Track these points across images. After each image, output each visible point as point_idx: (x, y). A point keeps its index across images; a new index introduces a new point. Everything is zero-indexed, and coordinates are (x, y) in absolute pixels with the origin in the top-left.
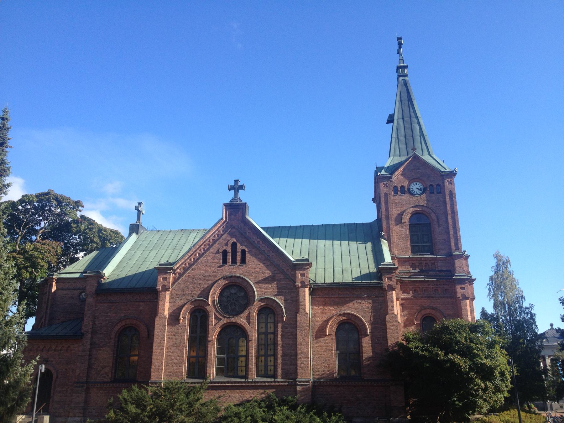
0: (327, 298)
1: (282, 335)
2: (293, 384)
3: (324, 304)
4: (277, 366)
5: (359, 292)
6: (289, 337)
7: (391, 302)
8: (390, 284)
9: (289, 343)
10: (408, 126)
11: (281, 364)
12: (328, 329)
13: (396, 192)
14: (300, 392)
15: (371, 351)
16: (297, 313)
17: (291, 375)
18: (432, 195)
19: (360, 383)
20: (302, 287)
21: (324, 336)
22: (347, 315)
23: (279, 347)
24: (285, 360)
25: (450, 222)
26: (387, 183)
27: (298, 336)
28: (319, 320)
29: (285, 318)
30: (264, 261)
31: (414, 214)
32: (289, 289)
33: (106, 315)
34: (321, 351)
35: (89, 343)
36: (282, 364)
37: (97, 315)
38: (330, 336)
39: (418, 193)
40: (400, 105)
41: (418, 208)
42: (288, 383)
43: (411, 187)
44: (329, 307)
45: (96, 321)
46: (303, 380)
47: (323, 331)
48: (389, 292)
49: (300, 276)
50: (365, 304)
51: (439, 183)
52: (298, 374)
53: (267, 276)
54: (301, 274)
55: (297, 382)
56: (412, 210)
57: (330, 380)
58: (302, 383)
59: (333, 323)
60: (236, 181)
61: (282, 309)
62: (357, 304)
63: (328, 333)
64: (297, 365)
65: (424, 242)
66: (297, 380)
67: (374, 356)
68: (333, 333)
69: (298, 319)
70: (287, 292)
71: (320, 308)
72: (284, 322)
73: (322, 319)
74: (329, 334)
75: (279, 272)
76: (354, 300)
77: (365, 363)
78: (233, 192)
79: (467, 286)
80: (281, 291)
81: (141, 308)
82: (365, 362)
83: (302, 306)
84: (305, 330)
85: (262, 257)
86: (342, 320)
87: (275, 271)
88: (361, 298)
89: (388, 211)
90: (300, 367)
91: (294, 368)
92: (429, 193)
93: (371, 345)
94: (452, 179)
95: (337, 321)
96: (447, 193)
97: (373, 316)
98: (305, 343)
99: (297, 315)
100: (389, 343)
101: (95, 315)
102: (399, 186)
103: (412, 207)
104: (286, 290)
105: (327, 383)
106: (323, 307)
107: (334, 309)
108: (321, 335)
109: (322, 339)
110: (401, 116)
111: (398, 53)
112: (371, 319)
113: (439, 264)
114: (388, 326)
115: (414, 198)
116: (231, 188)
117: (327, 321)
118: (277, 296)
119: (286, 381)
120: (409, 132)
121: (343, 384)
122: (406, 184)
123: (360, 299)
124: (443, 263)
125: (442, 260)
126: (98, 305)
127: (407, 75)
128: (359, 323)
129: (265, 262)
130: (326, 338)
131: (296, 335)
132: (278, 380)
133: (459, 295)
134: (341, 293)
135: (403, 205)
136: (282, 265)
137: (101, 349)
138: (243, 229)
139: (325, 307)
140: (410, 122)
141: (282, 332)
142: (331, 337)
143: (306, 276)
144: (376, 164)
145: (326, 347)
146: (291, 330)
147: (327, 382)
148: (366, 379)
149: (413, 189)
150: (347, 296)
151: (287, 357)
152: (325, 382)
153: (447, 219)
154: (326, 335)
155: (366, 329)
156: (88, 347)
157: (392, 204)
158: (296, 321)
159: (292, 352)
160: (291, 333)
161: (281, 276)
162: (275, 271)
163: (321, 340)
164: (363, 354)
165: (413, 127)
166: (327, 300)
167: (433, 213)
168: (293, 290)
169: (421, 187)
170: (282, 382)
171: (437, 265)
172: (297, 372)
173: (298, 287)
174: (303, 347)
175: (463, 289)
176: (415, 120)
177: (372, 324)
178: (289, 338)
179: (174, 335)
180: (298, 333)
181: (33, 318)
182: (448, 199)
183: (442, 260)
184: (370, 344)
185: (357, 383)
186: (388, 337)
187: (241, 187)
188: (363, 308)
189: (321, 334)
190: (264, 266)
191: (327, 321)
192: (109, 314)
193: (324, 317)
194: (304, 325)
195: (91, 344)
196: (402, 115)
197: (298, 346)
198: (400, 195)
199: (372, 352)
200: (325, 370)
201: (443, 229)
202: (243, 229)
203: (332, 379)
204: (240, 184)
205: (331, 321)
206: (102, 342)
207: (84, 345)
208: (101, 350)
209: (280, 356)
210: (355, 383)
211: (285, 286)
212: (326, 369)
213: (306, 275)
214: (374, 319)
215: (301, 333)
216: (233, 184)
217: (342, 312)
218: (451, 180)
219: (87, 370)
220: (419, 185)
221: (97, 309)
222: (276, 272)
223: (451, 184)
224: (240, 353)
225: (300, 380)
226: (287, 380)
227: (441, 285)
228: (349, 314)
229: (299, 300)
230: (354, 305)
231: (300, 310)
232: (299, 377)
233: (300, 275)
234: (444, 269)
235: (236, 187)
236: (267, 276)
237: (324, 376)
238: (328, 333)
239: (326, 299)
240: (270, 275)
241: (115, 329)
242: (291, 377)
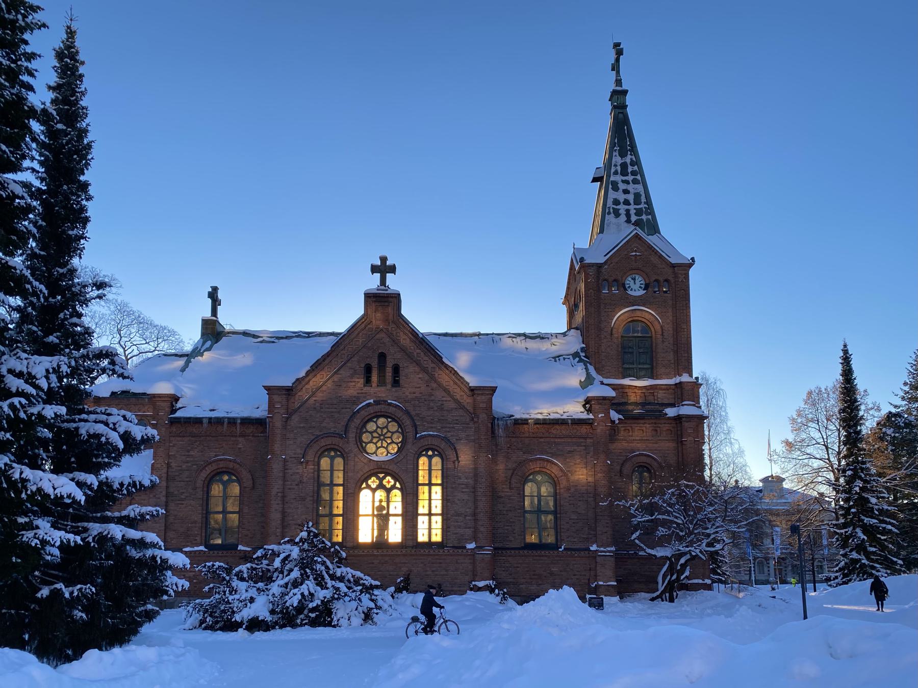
6: (464, 490)
32: (462, 424)
33: (187, 453)
35: (164, 493)
37: (173, 453)
43: (628, 282)
45: (171, 463)
60: (384, 259)
65: (640, 364)
78: (377, 276)
81: (240, 446)
101: (170, 454)
108: (503, 488)
111: (613, 69)
113: (659, 396)
116: (374, 269)
124: (665, 393)
125: (664, 389)
126: (172, 439)
137: (183, 502)
138: (395, 334)
144: (846, 360)
146: (466, 480)
151: (461, 518)
156: (164, 499)
159: (468, 510)
168: (469, 426)
169: (630, 279)
178: (463, 492)
179: (297, 485)
181: (131, 456)
187: (393, 269)
189: (504, 486)
192: (192, 453)
195: (167, 496)
202: (395, 334)
204: (379, 263)
206: (184, 493)
207: (157, 496)
208: (183, 504)
211: (457, 420)
216: (378, 262)
219: (527, 526)
221: (171, 444)
222: (444, 399)
224: (336, 512)
235: (384, 269)
241: (202, 474)
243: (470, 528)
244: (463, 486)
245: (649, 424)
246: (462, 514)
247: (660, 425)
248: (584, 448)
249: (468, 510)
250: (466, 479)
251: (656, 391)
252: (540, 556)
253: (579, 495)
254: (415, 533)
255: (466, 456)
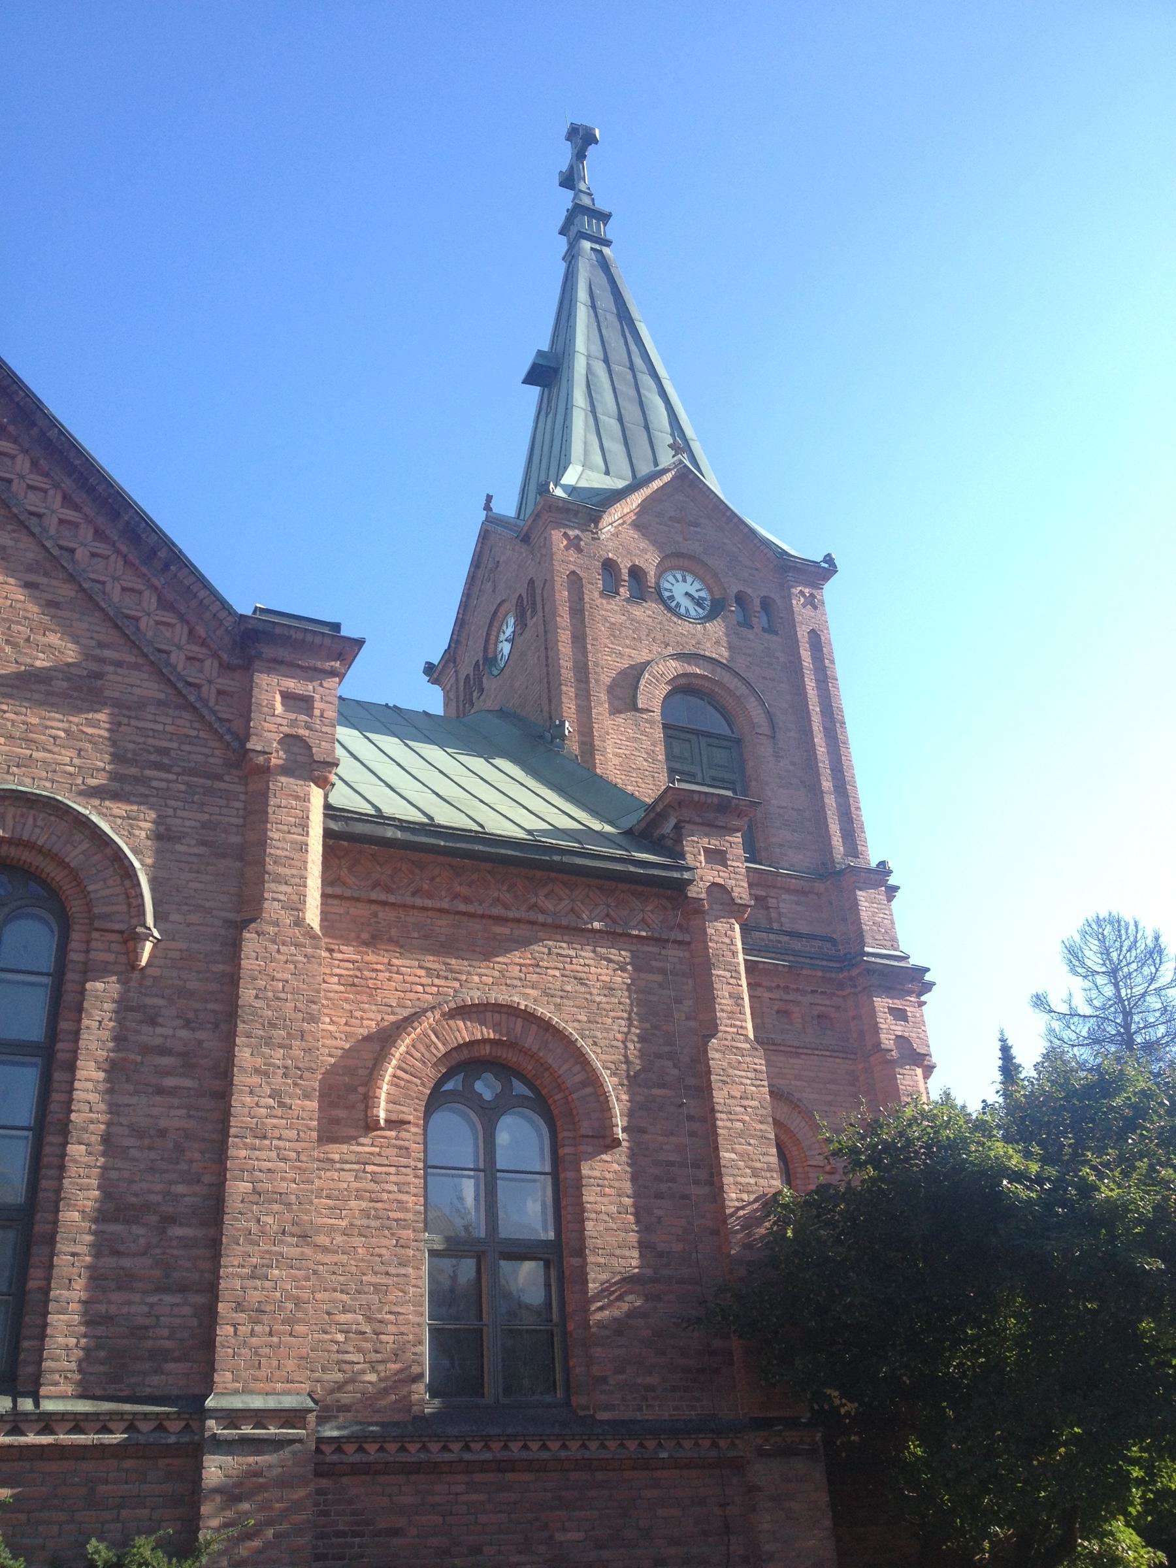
0: (384, 903)
1: (115, 1070)
2: (172, 1439)
3: (365, 936)
4: (47, 1290)
5: (561, 899)
6: (170, 1082)
7: (728, 974)
8: (721, 881)
9: (163, 1123)
10: (627, 390)
11: (79, 1284)
12: (385, 1087)
13: (610, 590)
14: (231, 1494)
15: (633, 1238)
16: (244, 924)
17: (158, 1371)
18: (745, 632)
19: (574, 1445)
20: (286, 771)
21: (352, 1132)
22: (497, 1016)
23: (76, 1150)
24: (117, 1253)
25: (819, 740)
26: (577, 537)
27: (241, 1079)
28: (331, 1028)
29: (148, 946)
30: (30, 569)
31: (683, 688)
32: (192, 772)
34: (332, 1229)
36: (97, 1278)
38: (393, 1134)
39: (693, 613)
40: (593, 320)
41: (697, 666)
42: (131, 1428)
44: (395, 961)
46: (257, 1403)
47: (352, 1097)
48: (716, 920)
49: (279, 708)
50: (593, 969)
51: (773, 596)
52: (223, 1354)
53: (42, 662)
54: (287, 696)
55: (211, 1423)
56: (675, 669)
57: (382, 1425)
58: (247, 1430)
59: (418, 1055)
61: (139, 885)
62: (551, 965)
63: (382, 1115)
64: (212, 1290)
66: (210, 1403)
67: (649, 1272)
68: (413, 1113)
69: (249, 964)
70: (182, 787)
71: (340, 956)
72: (136, 975)
73: (346, 1024)
74: (386, 1121)
75: (133, 659)
76: (537, 940)
77: (598, 1316)
79: (907, 1004)
80: (133, 771)
82: (601, 1309)
83: (284, 888)
84: (296, 1043)
85: (21, 545)
86: (472, 1043)
87: (101, 645)
88: (575, 932)
89: (585, 648)
90: (239, 1307)
91: (187, 1310)
92: (735, 623)
93: (634, 1205)
94: (815, 592)
95: (440, 1045)
96: (802, 633)
97: (638, 1036)
98: (287, 1133)
99: (246, 935)
100: (732, 1197)
102: (624, 565)
103: (678, 657)
104: (172, 777)
105: (360, 1449)
106: (359, 953)
107: (422, 972)
109: (344, 1148)
110: (597, 350)
112: (626, 1056)
113: (784, 908)
114: (719, 1096)
115: (684, 627)
117: (385, 1039)
118: (102, 799)
119: (111, 1414)
120: (632, 413)
121: (467, 1456)
122: (650, 561)
123: (566, 938)
124: (798, 903)
125: (795, 892)
127: (607, 243)
128: (564, 1068)
129: (33, 578)
130: (365, 1146)
131: (224, 1070)
132: (48, 1406)
133: (887, 1041)
134: (463, 890)
135: (640, 640)
136: (158, 623)
139: (371, 958)
140: (633, 380)
141: (115, 1039)
142: (397, 1138)
143: (317, 712)
145: (364, 1205)
146: (184, 1034)
147: (360, 1441)
148: (603, 1416)
149: (675, 594)
150: (497, 911)
151: (137, 1230)
152: (348, 1439)
153: (807, 733)
154: (370, 1126)
155: (606, 1108)
157: (598, 631)
158: (232, 980)
159: (180, 1189)
160: (184, 1055)
161: (148, 687)
162: (101, 645)
163: (336, 1157)
164: (591, 1259)
165: (643, 399)
166: (386, 915)
167: (753, 699)
170: (77, 1423)
171: (778, 908)
172: (207, 1344)
173: (265, 771)
174: (266, 1159)
175: (900, 1015)
176: (646, 380)
177: (633, 1082)
178: (160, 1091)
180: (244, 1055)
182: (806, 655)
183: (795, 892)
184: (628, 1201)
185: (554, 1445)
186: (723, 1162)
188: (583, 989)
190: (36, 600)
191: (385, 1039)
193: (358, 1014)
194: (290, 1005)
196: (600, 348)
197: (232, 1152)
198: (627, 600)
199: (643, 1246)
200: (348, 1357)
201: (791, 768)
203: (397, 1424)
205: (407, 1041)
209: (76, 1215)
210: (544, 1447)
211: (165, 752)
212: (359, 1350)
213: (317, 704)
214: (642, 1054)
215: (263, 1055)
217: (473, 996)
218: (812, 595)
220: (693, 586)
222: (108, 653)
223: (815, 608)
225: (237, 1403)
226: (127, 1407)
227: (803, 992)
228: (511, 1011)
229: (262, 843)
230: (538, 966)
231: (266, 905)
232: (223, 1378)
233: (278, 698)
234: (803, 928)
236: (38, 664)
237: (345, 1398)
238: (382, 1115)
239: (375, 915)
240: (68, 665)
242: (155, 1383)
243: (183, 1289)
244: (166, 1061)
245: (769, 989)
246: (147, 1207)
247: (800, 998)
248: (658, 978)
249: (180, 1189)
250: (187, 1024)
251: (773, 892)
252: (503, 1466)
253: (655, 1171)
254: (728, 514)
255: (194, 918)
